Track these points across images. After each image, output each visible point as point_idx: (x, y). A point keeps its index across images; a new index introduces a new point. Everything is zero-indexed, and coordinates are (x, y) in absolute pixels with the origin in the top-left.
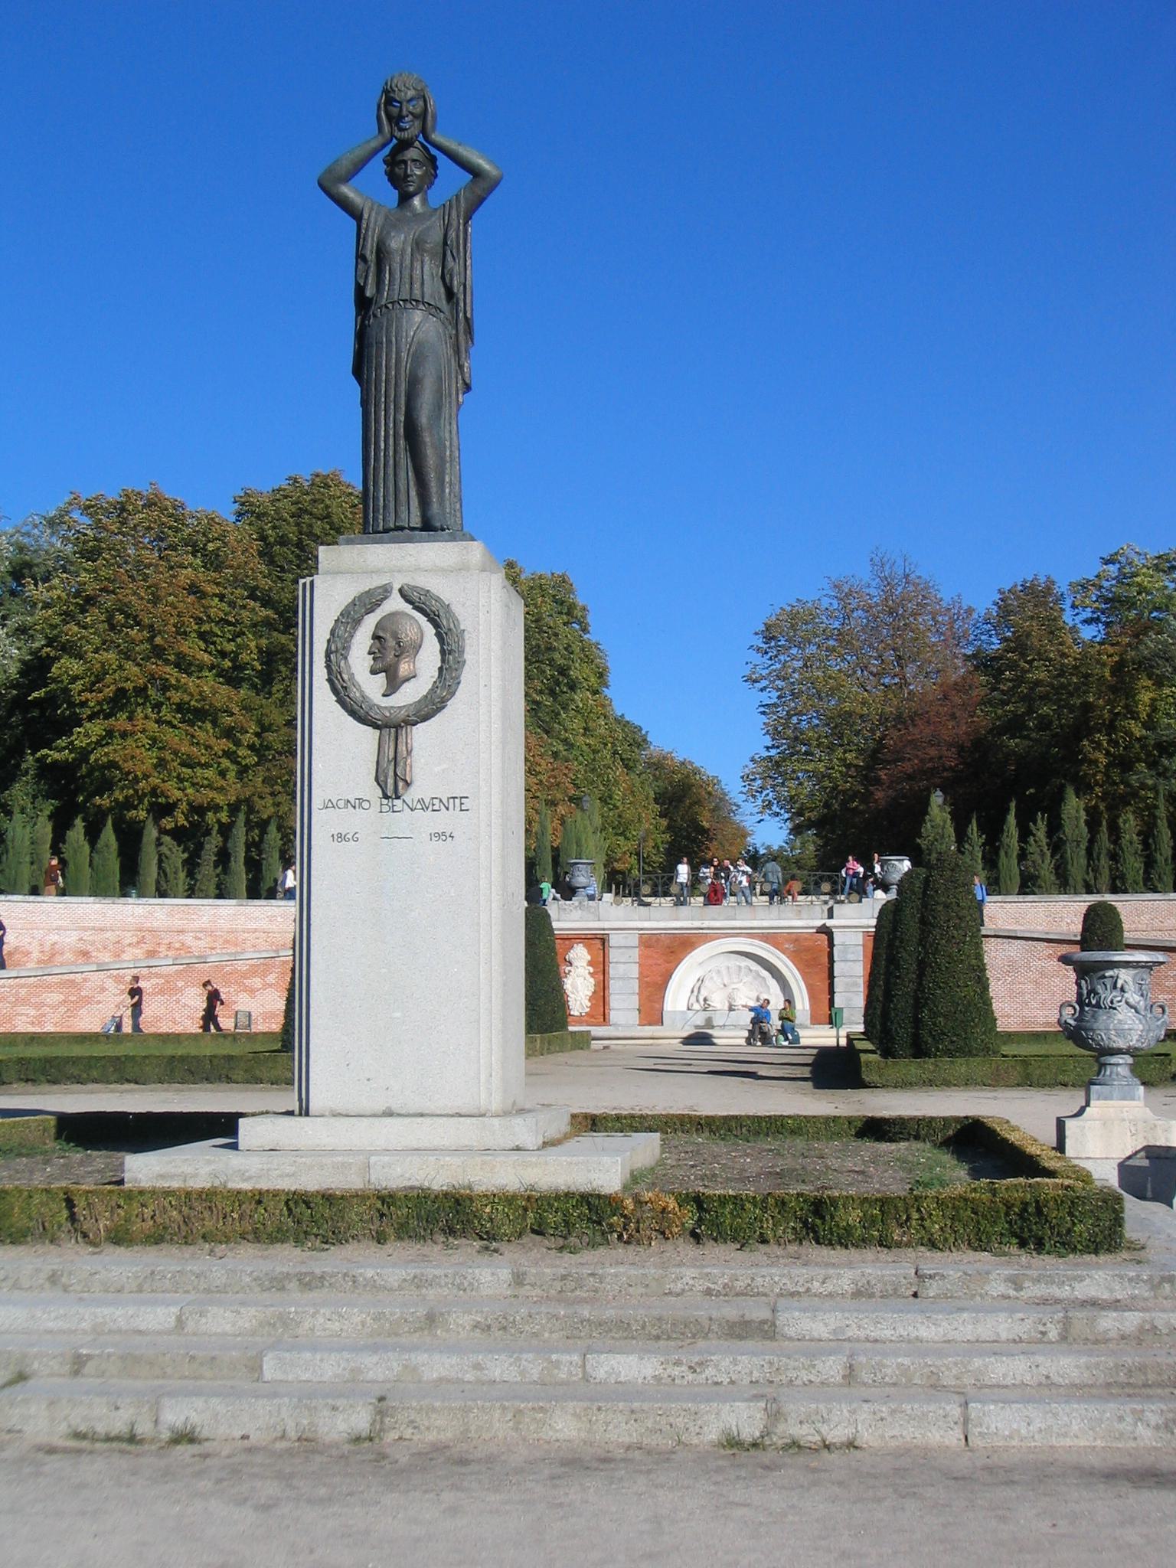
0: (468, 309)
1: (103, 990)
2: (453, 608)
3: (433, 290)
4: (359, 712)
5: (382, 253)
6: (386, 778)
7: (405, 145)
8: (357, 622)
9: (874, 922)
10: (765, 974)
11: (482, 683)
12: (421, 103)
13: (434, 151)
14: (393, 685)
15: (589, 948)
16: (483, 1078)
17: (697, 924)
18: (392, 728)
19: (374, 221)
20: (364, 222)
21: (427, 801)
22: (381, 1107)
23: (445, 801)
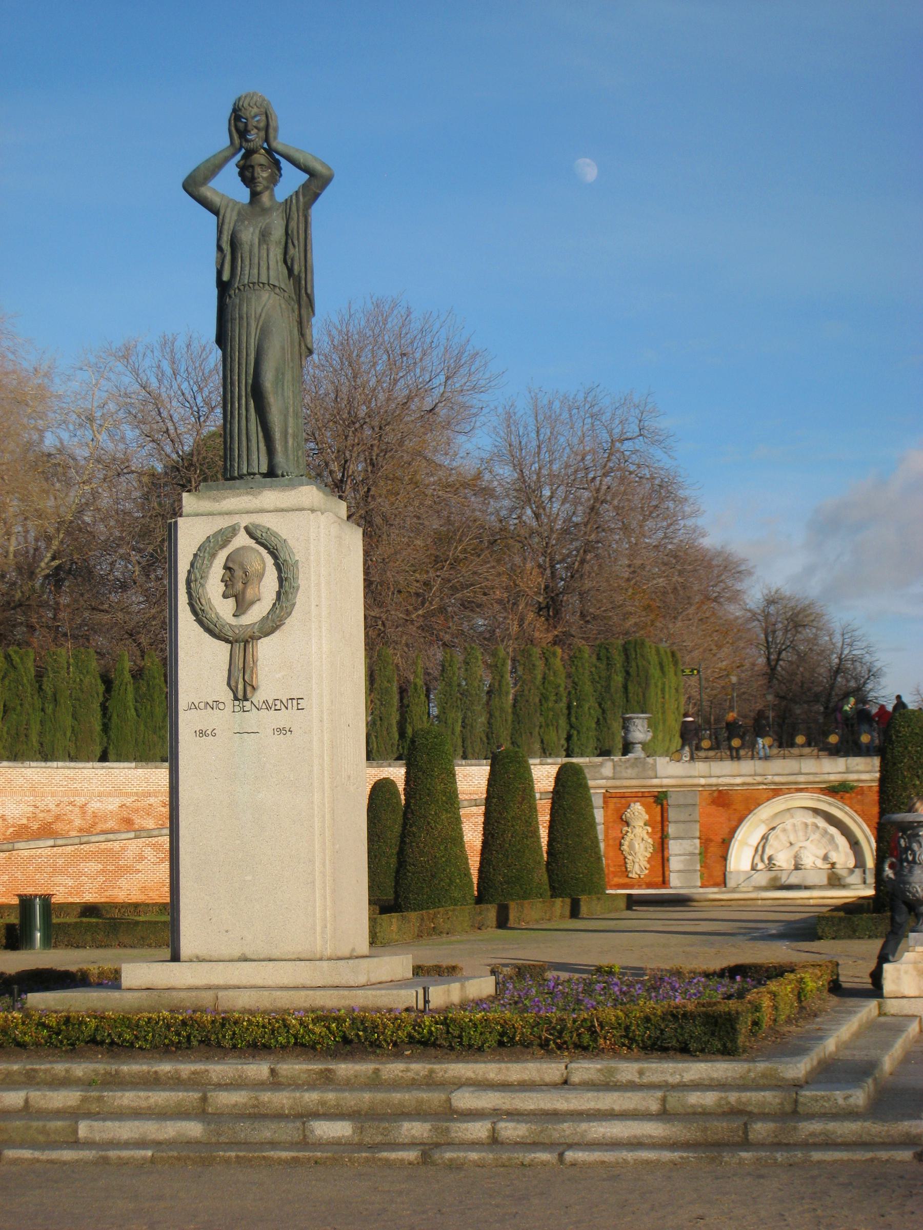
0: (309, 286)
1: (142, 858)
2: (289, 541)
3: (276, 272)
5: (234, 244)
6: (237, 683)
7: (251, 142)
8: (213, 556)
9: (878, 775)
10: (833, 830)
11: (314, 604)
12: (264, 118)
13: (277, 157)
14: (242, 606)
16: (318, 929)
18: (241, 643)
19: (231, 218)
20: (221, 217)
21: (270, 702)
22: (237, 954)
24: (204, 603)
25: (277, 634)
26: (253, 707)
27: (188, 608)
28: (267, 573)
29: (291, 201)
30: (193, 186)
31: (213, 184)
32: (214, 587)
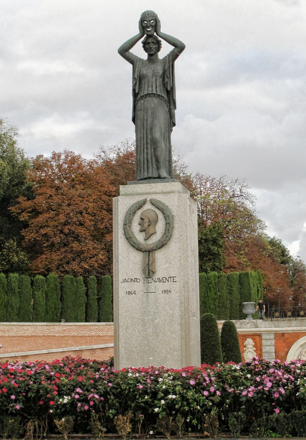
4: (138, 248)
13: (160, 39)
15: (254, 340)
17: (299, 328)
18: (148, 252)
20: (135, 65)
21: (161, 279)
23: (167, 278)
24: (130, 234)
25: (163, 248)
26: (153, 281)
27: (123, 237)
28: (159, 220)
29: (166, 58)
30: (124, 52)
31: (131, 51)
32: (136, 227)
